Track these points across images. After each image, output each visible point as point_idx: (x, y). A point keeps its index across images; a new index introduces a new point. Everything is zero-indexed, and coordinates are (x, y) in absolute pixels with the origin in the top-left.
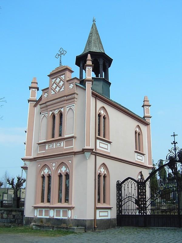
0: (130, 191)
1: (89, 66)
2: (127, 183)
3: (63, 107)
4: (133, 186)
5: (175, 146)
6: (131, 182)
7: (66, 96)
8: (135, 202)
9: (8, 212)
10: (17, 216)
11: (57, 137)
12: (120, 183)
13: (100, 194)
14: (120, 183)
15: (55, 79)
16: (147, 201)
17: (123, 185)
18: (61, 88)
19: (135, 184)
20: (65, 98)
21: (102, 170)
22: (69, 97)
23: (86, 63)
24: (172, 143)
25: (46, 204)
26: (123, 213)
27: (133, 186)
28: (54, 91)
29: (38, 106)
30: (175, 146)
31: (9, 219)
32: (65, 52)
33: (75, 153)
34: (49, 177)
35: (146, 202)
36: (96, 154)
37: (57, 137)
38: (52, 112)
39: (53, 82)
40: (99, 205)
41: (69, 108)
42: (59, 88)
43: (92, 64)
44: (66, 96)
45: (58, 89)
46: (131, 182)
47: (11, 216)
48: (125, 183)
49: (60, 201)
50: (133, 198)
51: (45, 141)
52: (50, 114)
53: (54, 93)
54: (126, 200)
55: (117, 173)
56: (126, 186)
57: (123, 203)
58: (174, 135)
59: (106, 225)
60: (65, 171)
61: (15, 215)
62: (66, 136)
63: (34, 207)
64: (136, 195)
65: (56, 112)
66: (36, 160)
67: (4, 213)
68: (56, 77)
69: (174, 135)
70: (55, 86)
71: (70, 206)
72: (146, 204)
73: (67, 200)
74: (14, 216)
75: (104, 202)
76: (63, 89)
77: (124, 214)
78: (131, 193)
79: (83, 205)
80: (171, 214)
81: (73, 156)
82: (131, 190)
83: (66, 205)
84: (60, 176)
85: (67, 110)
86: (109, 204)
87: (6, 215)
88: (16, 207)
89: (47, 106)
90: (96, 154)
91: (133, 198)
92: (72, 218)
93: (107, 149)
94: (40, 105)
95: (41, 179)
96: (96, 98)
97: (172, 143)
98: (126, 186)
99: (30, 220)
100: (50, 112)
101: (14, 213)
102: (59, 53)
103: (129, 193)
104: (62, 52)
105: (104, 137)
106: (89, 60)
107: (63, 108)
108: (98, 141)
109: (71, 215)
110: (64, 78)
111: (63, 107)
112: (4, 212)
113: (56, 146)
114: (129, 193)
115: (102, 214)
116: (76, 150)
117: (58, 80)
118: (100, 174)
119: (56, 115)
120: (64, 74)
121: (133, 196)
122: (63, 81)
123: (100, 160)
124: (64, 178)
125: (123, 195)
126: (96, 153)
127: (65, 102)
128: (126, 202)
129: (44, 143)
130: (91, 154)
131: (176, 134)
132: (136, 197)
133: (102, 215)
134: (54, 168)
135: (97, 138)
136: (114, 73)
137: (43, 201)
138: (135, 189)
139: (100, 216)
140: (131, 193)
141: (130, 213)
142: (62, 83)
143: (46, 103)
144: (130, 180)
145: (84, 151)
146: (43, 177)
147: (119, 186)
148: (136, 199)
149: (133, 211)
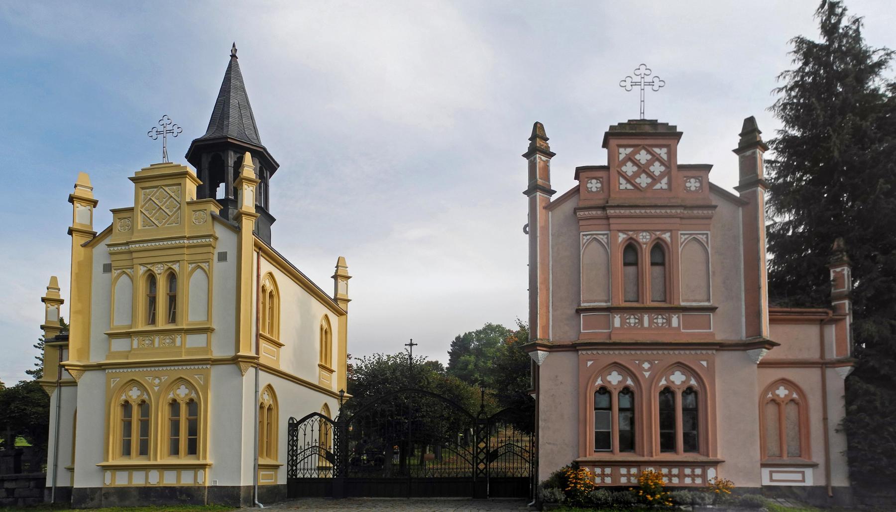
13: (264, 443)
21: (267, 400)
25: (136, 460)
26: (300, 475)
33: (721, 346)
36: (259, 367)
37: (162, 324)
38: (166, 267)
40: (262, 461)
51: (603, 304)
53: (629, 187)
54: (308, 452)
55: (294, 403)
56: (309, 428)
57: (300, 457)
58: (411, 345)
59: (270, 495)
62: (683, 304)
63: (103, 466)
66: (105, 369)
69: (411, 345)
71: (201, 462)
73: (193, 449)
79: (233, 459)
81: (714, 352)
89: (131, 252)
90: (259, 367)
94: (109, 246)
98: (309, 428)
100: (620, 234)
102: (161, 129)
104: (169, 127)
105: (271, 331)
108: (261, 341)
109: (207, 479)
113: (623, 322)
115: (776, 476)
116: (719, 337)
118: (262, 403)
120: (180, 184)
123: (265, 379)
124: (183, 409)
125: (300, 443)
126: (258, 364)
127: (678, 220)
131: (409, 342)
133: (266, 479)
134: (647, 374)
135: (259, 336)
141: (308, 476)
144: (316, 417)
145: (235, 360)
147: (293, 427)
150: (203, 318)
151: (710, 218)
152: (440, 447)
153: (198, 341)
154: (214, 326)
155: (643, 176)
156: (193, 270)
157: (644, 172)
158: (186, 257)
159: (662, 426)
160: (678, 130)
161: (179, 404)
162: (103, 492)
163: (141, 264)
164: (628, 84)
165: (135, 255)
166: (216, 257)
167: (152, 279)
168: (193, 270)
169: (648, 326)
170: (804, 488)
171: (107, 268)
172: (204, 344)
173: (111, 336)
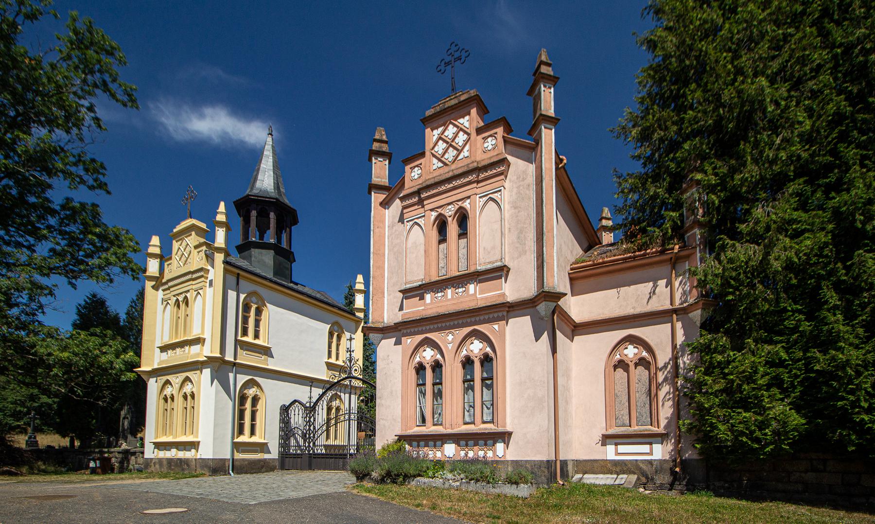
0: (296, 420)
3: (469, 197)
15: (441, 129)
18: (459, 151)
22: (195, 276)
28: (440, 160)
32: (464, 54)
34: (437, 366)
38: (457, 207)
39: (435, 138)
41: (411, 223)
42: (455, 152)
45: (452, 153)
52: (433, 218)
53: (440, 165)
65: (449, 212)
68: (445, 125)
70: (441, 146)
75: (253, 433)
76: (465, 152)
83: (490, 428)
84: (468, 362)
86: (197, 437)
99: (148, 463)
104: (457, 55)
106: (222, 213)
107: (468, 201)
110: (467, 124)
111: (469, 197)
117: (451, 131)
119: (428, 367)
122: (465, 132)
127: (475, 185)
134: (450, 346)
139: (617, 454)
142: (461, 138)
146: (420, 369)
147: (285, 410)
150: (199, 331)
153: (195, 349)
154: (507, 262)
155: (451, 149)
157: (451, 146)
158: (194, 287)
161: (473, 362)
164: (442, 67)
165: (425, 203)
166: (208, 284)
169: (476, 294)
170: (650, 462)
173: (408, 293)
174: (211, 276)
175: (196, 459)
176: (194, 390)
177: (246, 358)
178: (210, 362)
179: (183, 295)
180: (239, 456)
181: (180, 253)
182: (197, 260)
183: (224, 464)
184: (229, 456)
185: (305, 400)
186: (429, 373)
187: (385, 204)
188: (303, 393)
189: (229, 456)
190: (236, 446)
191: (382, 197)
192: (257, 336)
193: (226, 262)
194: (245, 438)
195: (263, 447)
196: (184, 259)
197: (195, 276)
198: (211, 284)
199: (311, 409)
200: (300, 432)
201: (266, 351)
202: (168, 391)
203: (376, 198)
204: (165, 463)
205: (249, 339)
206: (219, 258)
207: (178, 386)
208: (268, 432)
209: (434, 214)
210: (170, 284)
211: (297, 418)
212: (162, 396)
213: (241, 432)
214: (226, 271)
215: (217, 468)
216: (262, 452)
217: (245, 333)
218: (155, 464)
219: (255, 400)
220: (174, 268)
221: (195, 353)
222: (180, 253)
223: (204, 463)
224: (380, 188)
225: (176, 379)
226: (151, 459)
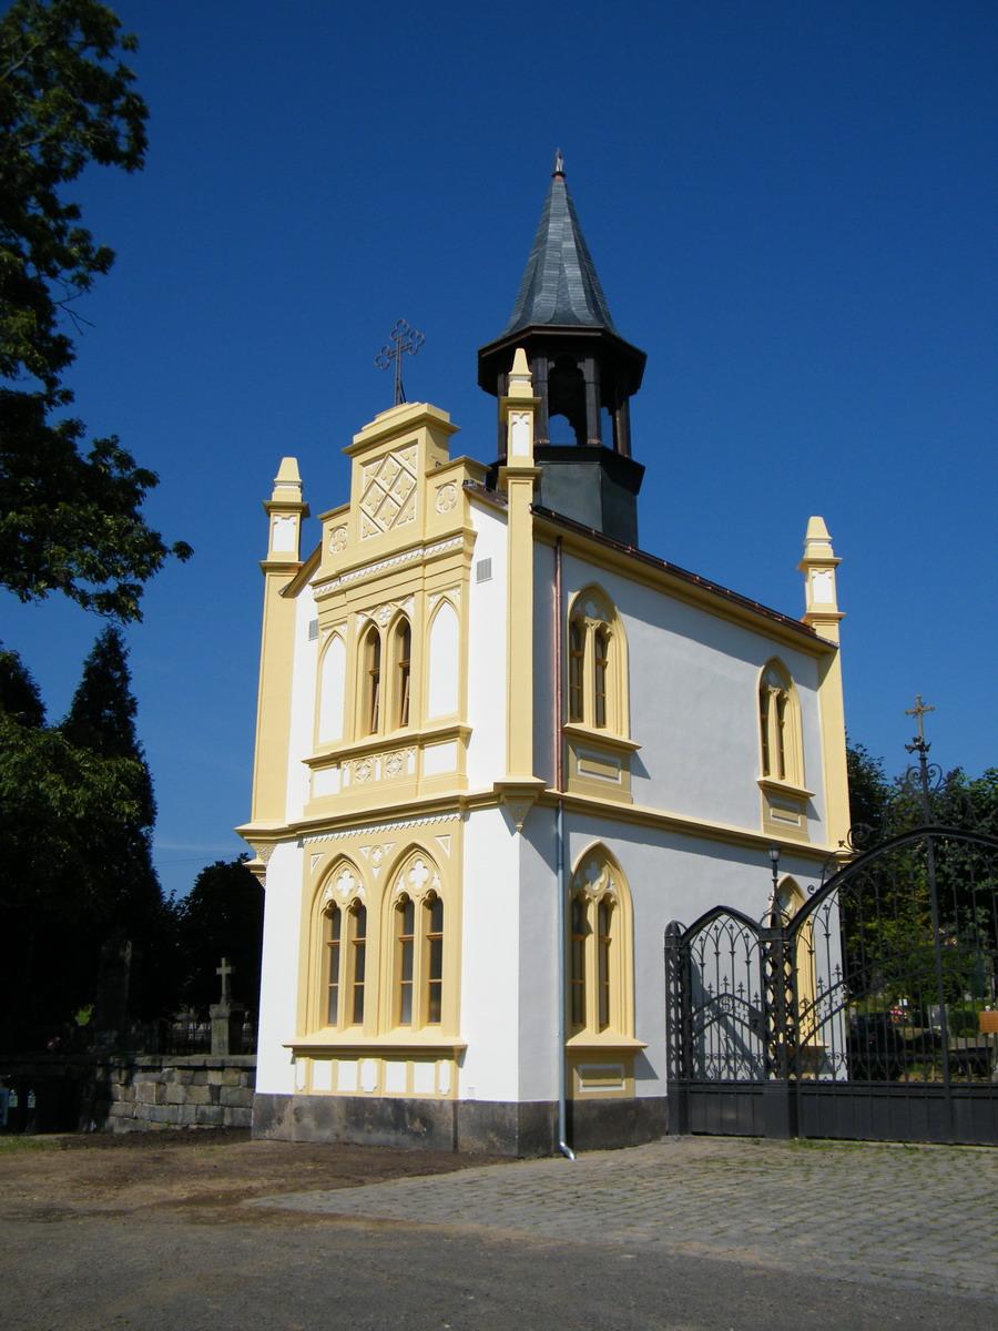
0: (725, 971)
1: (521, 404)
2: (713, 932)
3: (412, 594)
4: (740, 943)
5: (923, 759)
6: (731, 927)
7: (424, 545)
8: (747, 1021)
9: (190, 1073)
10: (229, 1090)
11: (389, 733)
12: (683, 931)
14: (683, 931)
16: (802, 1017)
17: (696, 944)
19: (747, 936)
20: (421, 551)
22: (431, 552)
23: (271, 499)
24: (907, 747)
27: (740, 943)
29: (308, 592)
30: (923, 759)
31: (193, 1107)
34: (359, 910)
35: (798, 1020)
38: (365, 619)
43: (534, 395)
44: (424, 545)
46: (731, 927)
47: (204, 1094)
48: (702, 934)
49: (404, 1014)
50: (741, 1000)
52: (359, 627)
56: (710, 947)
60: (351, 891)
61: (219, 1087)
64: (756, 987)
65: (383, 618)
67: (171, 1080)
72: (796, 1030)
74: (215, 1091)
77: (732, 1078)
78: (729, 981)
80: (821, 1077)
82: (731, 966)
84: (405, 905)
85: (432, 606)
87: (181, 1087)
88: (227, 1050)
91: (741, 1000)
92: (462, 1096)
93: (617, 779)
95: (320, 923)
96: (556, 548)
97: (907, 747)
98: (710, 947)
100: (360, 616)
101: (214, 1078)
103: (722, 981)
107: (412, 600)
112: (169, 1073)
114: (722, 981)
119: (383, 632)
121: (738, 995)
124: (421, 914)
128: (821, 1025)
129: (336, 759)
130: (535, 804)
132: (753, 998)
134: (376, 872)
136: (650, 423)
137: (331, 1018)
138: (748, 963)
140: (729, 981)
143: (337, 576)
144: (724, 918)
146: (333, 912)
147: (679, 943)
148: (754, 1005)
149: (723, 1062)
150: (454, 709)
151: (349, 508)
152: (111, 1036)
153: (440, 757)
154: (469, 724)
156: (438, 606)
159: (582, 987)
160: (154, 512)
161: (339, 910)
162: (294, 1105)
163: (357, 612)
166: (473, 574)
167: (374, 638)
168: (438, 606)
171: (314, 629)
172: (453, 767)
174: (480, 552)
175: (455, 1104)
176: (437, 885)
177: (589, 784)
178: (506, 796)
179: (390, 610)
180: (586, 1091)
181: (376, 493)
182: (444, 502)
183: (546, 1120)
184: (554, 1094)
185: (758, 905)
186: (346, 919)
187: (291, 592)
188: (752, 889)
189: (554, 1094)
190: (578, 1060)
191: (287, 579)
192: (600, 720)
193: (537, 509)
194: (588, 1037)
195: (627, 1060)
196: (390, 508)
197: (431, 552)
198: (485, 571)
199: (778, 941)
200: (742, 1012)
201: (622, 756)
202: (343, 889)
203: (275, 583)
204: (338, 1112)
205: (587, 725)
206: (520, 495)
207: (379, 874)
208: (634, 1015)
209: (362, 620)
210: (348, 580)
211: (731, 966)
212: (323, 904)
213: (331, 1018)
214: (538, 532)
215: (531, 1131)
216: (630, 1074)
217: (578, 715)
218: (298, 1113)
219: (606, 907)
220: (343, 543)
221: (434, 771)
222: (376, 493)
223: (487, 1115)
224: (283, 568)
225: (373, 849)
226: (284, 1099)
